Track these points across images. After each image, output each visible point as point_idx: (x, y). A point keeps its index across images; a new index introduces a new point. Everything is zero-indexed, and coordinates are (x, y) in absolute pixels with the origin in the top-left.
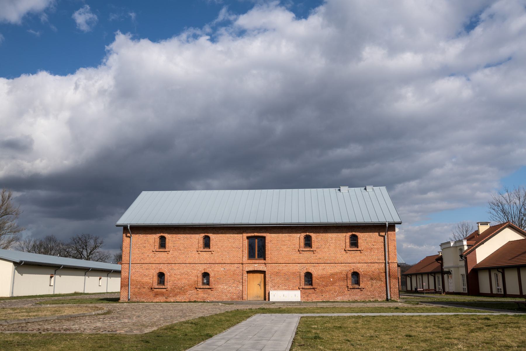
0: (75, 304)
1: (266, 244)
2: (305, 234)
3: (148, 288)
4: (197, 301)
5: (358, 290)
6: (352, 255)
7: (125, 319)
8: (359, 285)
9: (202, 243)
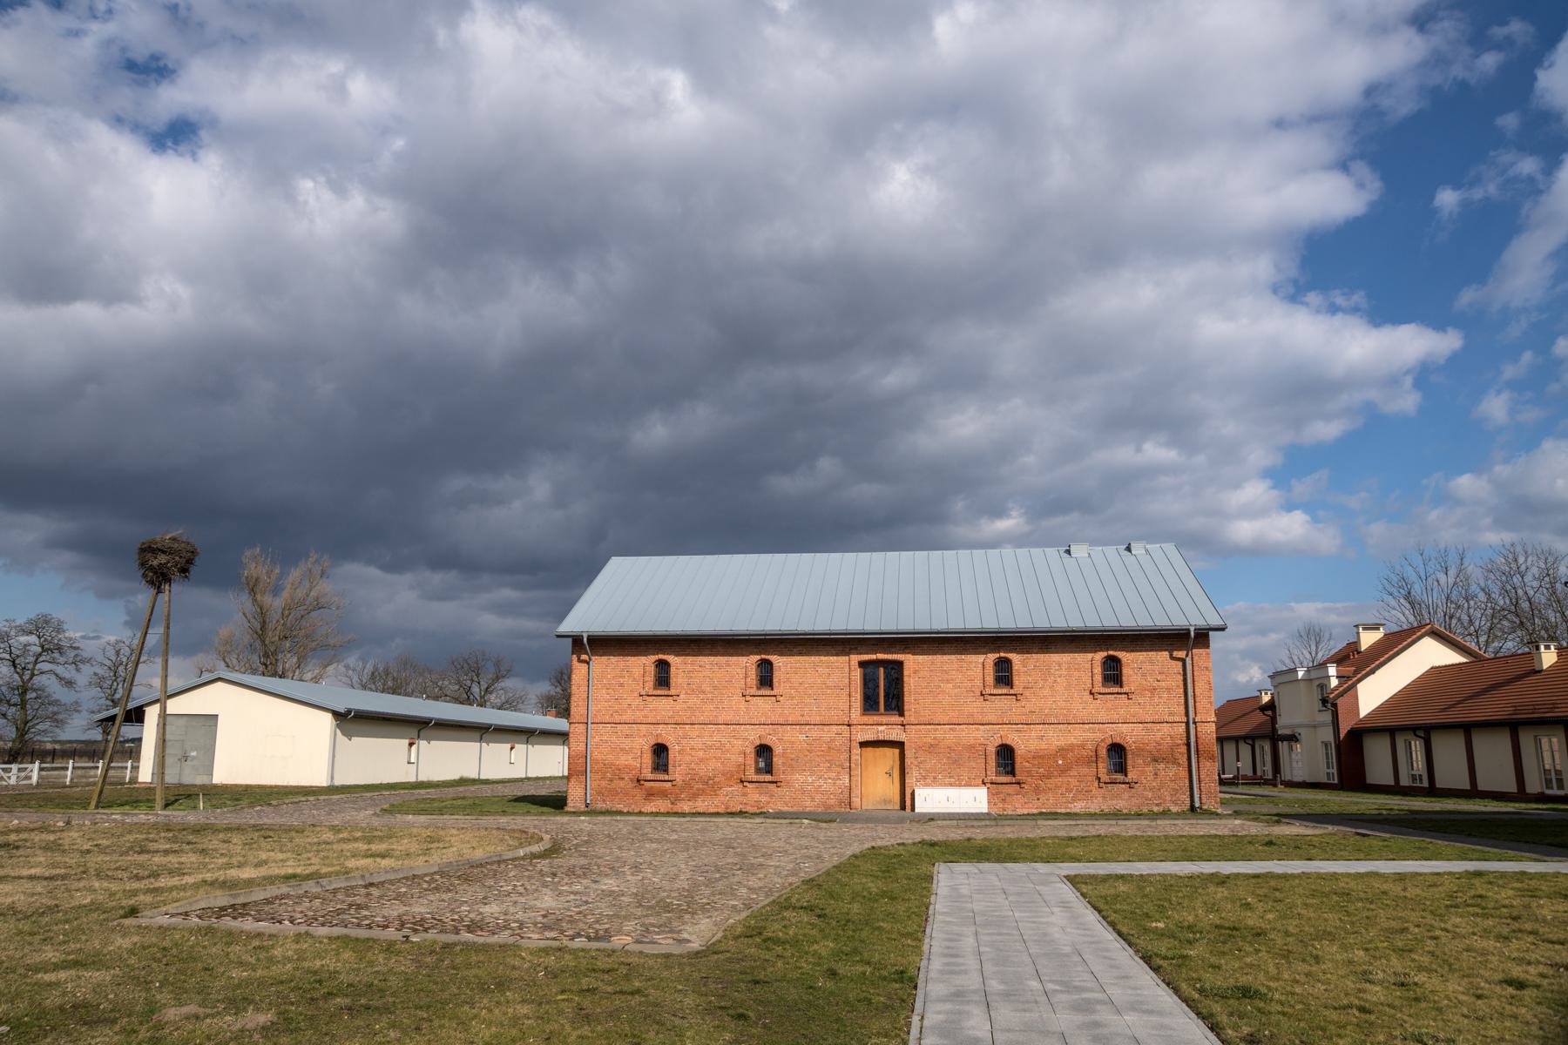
0: (468, 815)
1: (906, 679)
2: (997, 655)
3: (631, 780)
4: (746, 812)
5: (1124, 785)
6: (1109, 705)
7: (606, 875)
8: (1126, 775)
9: (754, 677)
